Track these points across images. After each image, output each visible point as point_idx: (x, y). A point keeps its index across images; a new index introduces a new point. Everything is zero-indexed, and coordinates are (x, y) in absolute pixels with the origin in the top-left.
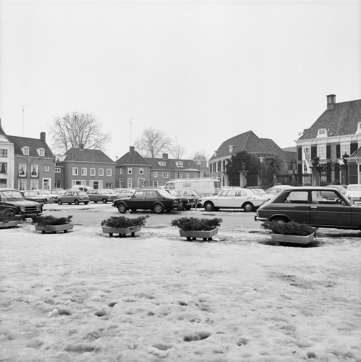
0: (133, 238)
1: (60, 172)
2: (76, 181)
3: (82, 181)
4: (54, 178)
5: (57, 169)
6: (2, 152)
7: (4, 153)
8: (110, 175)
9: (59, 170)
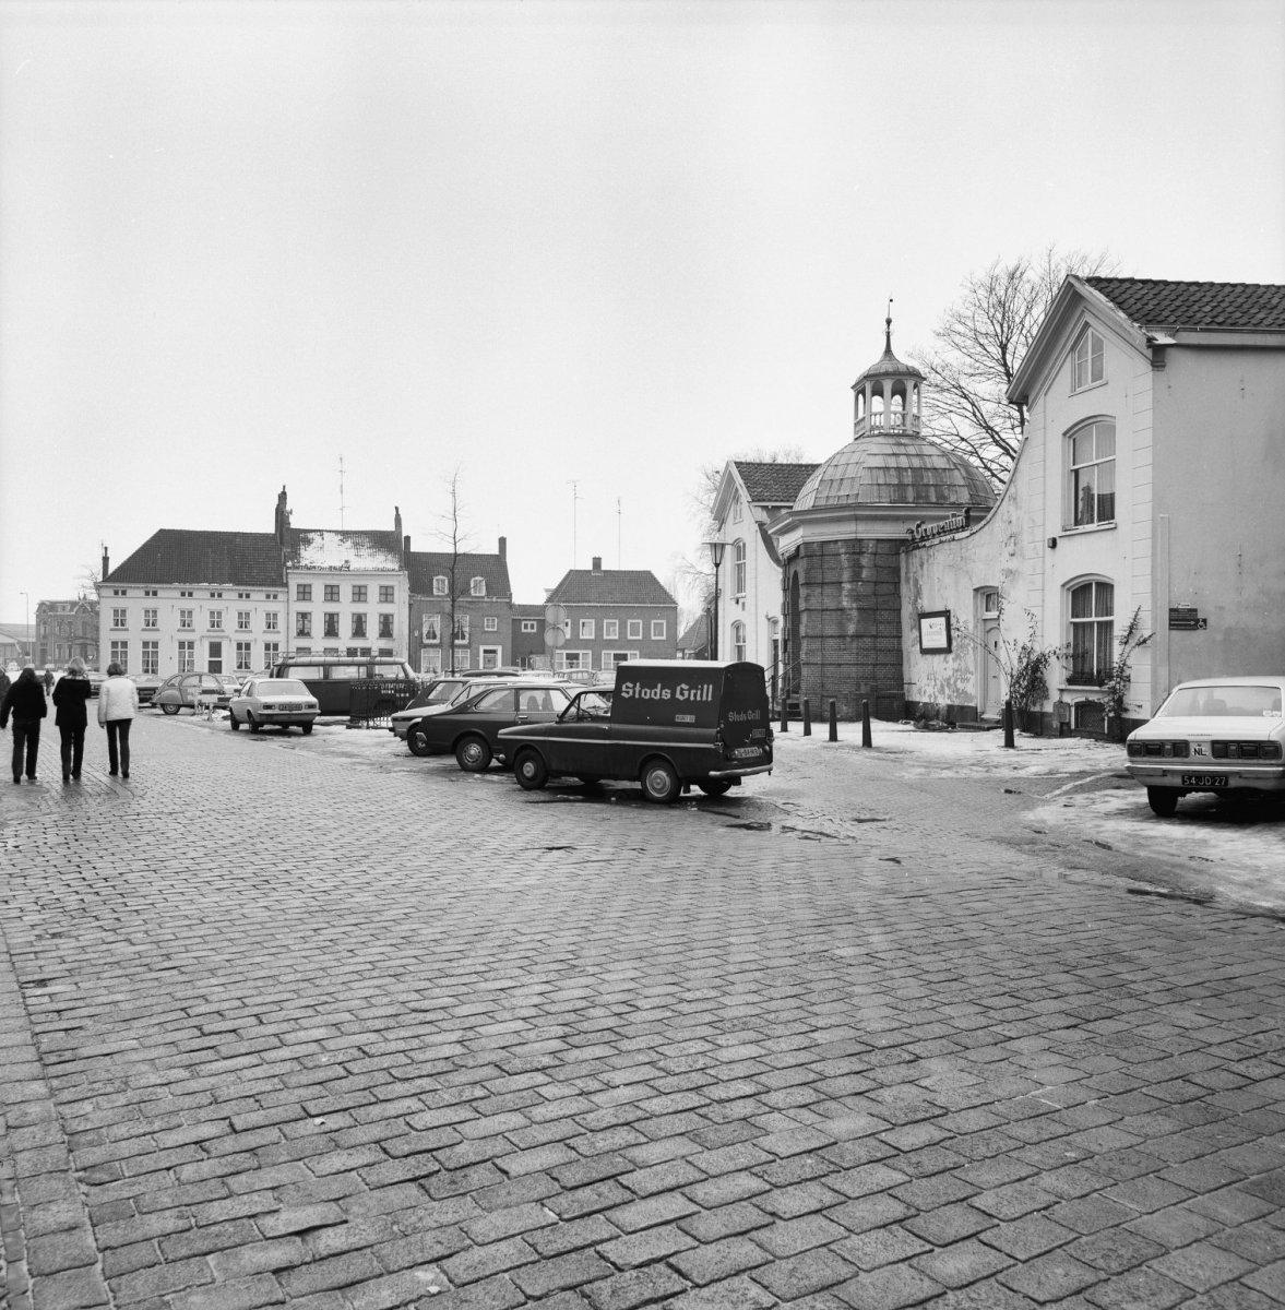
0: (675, 813)
1: (535, 630)
2: (613, 652)
3: (580, 652)
4: (510, 646)
5: (529, 623)
6: (357, 590)
7: (387, 595)
8: (631, 635)
9: (526, 626)
